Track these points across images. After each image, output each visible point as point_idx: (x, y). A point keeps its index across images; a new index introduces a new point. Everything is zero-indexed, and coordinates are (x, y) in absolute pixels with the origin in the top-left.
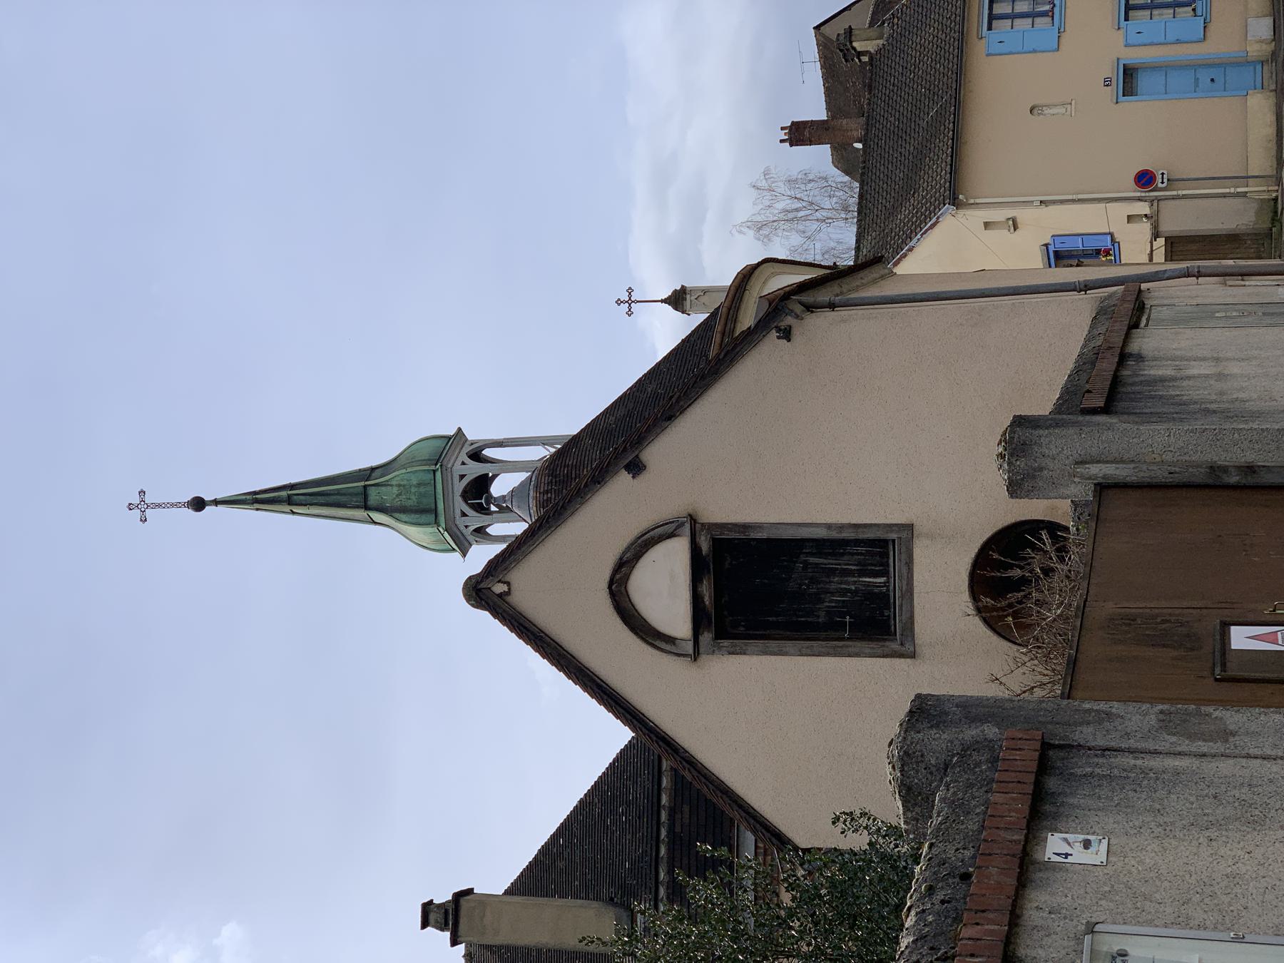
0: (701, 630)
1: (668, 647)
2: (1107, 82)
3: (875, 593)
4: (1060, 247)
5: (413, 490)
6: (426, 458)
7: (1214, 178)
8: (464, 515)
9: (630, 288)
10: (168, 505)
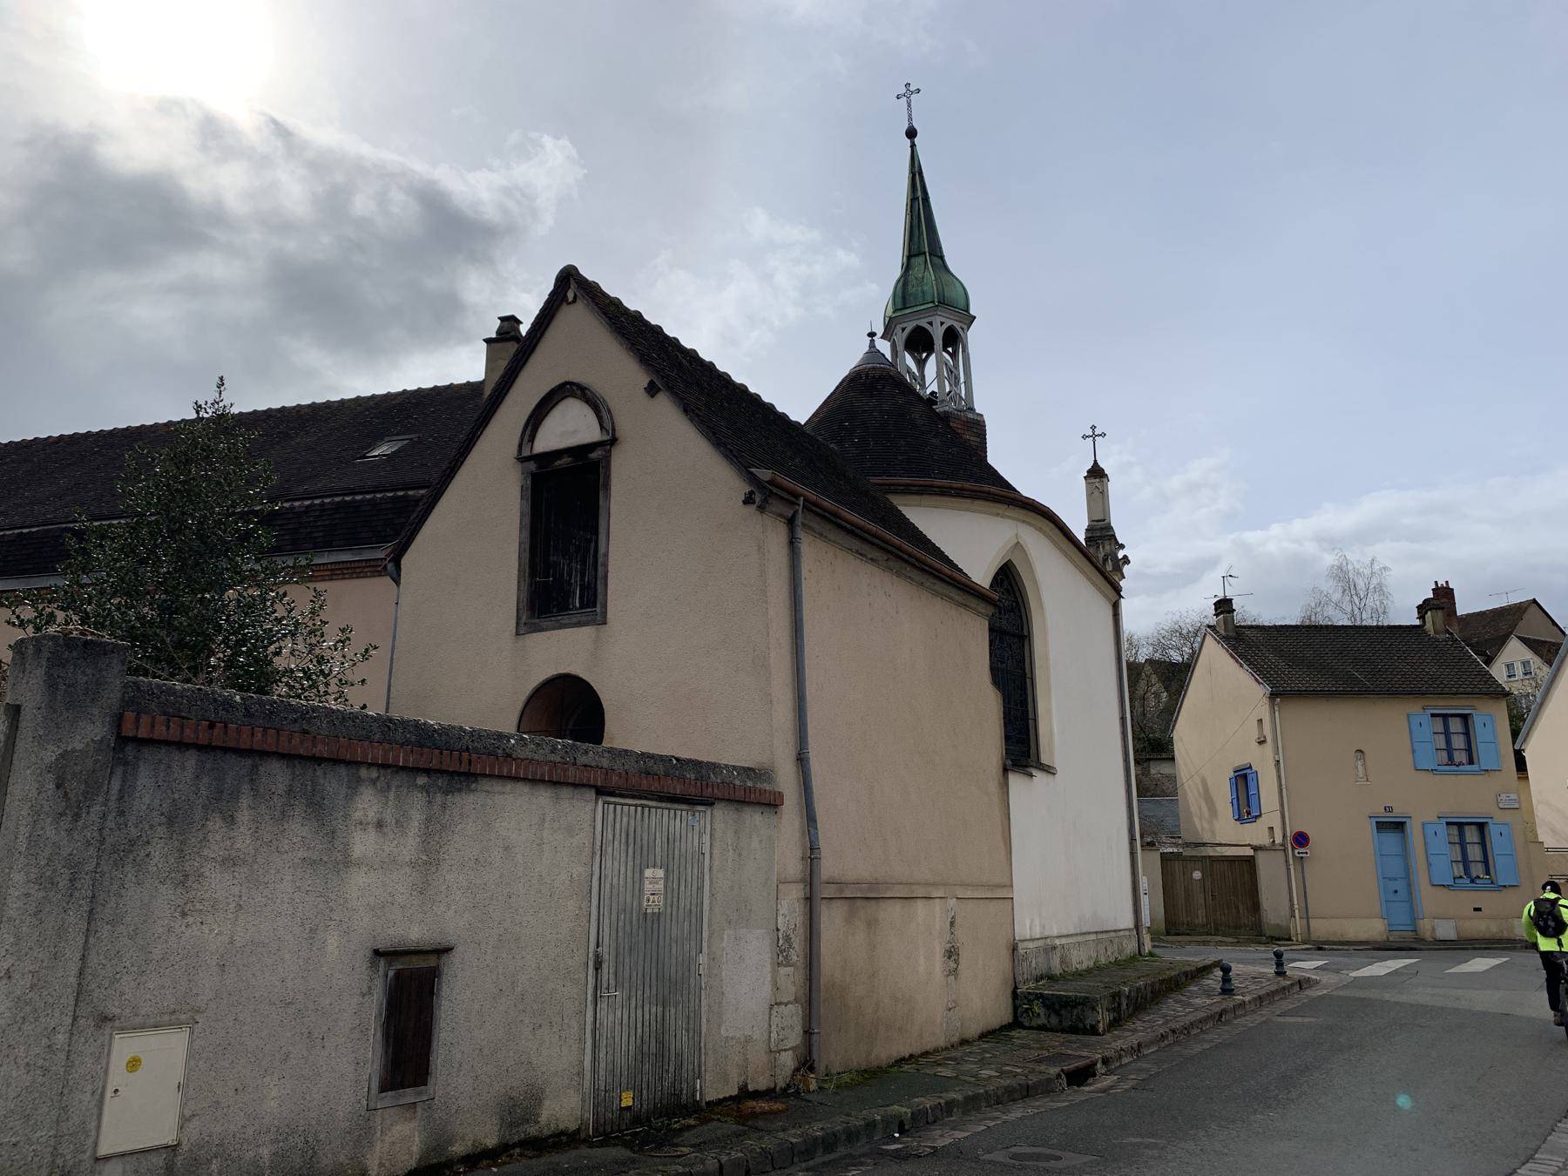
1: (526, 438)
2: (1388, 809)
4: (1249, 778)
5: (920, 289)
7: (1305, 892)
8: (903, 330)
9: (1105, 435)
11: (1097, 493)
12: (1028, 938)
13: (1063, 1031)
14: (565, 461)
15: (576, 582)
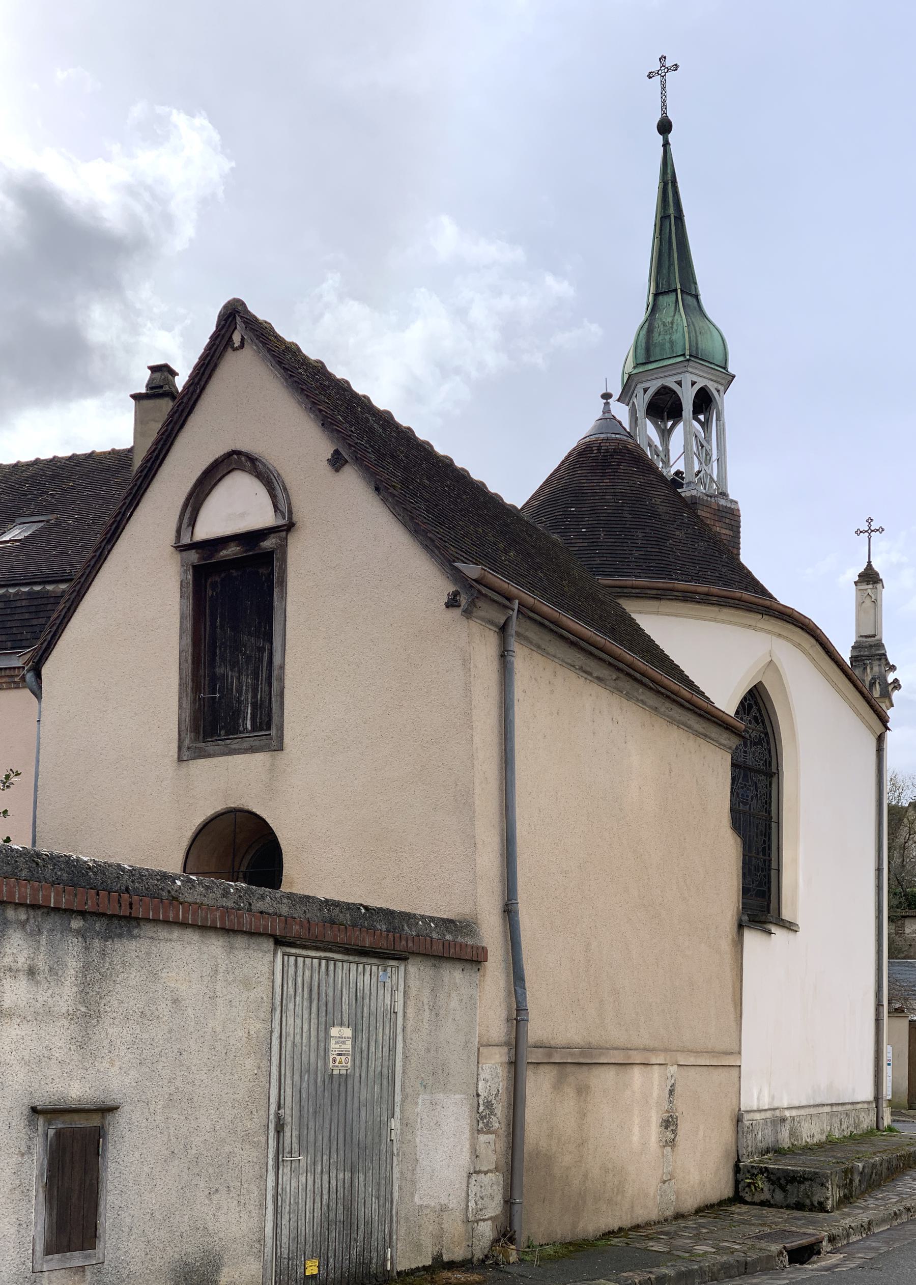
0: (200, 551)
1: (186, 521)
3: (238, 720)
5: (667, 337)
6: (700, 345)
8: (645, 390)
10: (664, 97)
11: (868, 602)
12: (755, 1108)
13: (788, 1207)
14: (231, 552)
15: (247, 699)
